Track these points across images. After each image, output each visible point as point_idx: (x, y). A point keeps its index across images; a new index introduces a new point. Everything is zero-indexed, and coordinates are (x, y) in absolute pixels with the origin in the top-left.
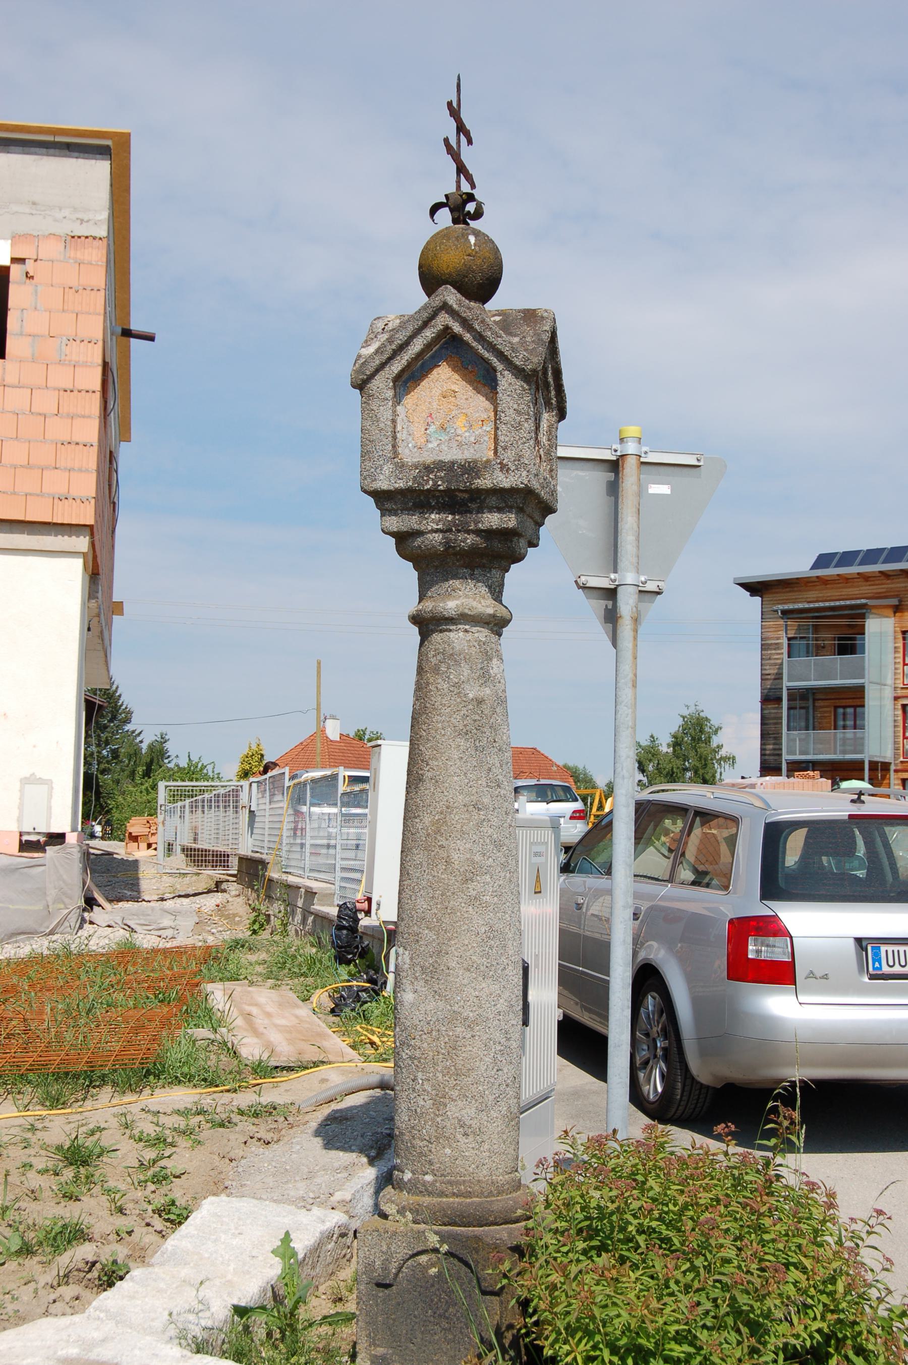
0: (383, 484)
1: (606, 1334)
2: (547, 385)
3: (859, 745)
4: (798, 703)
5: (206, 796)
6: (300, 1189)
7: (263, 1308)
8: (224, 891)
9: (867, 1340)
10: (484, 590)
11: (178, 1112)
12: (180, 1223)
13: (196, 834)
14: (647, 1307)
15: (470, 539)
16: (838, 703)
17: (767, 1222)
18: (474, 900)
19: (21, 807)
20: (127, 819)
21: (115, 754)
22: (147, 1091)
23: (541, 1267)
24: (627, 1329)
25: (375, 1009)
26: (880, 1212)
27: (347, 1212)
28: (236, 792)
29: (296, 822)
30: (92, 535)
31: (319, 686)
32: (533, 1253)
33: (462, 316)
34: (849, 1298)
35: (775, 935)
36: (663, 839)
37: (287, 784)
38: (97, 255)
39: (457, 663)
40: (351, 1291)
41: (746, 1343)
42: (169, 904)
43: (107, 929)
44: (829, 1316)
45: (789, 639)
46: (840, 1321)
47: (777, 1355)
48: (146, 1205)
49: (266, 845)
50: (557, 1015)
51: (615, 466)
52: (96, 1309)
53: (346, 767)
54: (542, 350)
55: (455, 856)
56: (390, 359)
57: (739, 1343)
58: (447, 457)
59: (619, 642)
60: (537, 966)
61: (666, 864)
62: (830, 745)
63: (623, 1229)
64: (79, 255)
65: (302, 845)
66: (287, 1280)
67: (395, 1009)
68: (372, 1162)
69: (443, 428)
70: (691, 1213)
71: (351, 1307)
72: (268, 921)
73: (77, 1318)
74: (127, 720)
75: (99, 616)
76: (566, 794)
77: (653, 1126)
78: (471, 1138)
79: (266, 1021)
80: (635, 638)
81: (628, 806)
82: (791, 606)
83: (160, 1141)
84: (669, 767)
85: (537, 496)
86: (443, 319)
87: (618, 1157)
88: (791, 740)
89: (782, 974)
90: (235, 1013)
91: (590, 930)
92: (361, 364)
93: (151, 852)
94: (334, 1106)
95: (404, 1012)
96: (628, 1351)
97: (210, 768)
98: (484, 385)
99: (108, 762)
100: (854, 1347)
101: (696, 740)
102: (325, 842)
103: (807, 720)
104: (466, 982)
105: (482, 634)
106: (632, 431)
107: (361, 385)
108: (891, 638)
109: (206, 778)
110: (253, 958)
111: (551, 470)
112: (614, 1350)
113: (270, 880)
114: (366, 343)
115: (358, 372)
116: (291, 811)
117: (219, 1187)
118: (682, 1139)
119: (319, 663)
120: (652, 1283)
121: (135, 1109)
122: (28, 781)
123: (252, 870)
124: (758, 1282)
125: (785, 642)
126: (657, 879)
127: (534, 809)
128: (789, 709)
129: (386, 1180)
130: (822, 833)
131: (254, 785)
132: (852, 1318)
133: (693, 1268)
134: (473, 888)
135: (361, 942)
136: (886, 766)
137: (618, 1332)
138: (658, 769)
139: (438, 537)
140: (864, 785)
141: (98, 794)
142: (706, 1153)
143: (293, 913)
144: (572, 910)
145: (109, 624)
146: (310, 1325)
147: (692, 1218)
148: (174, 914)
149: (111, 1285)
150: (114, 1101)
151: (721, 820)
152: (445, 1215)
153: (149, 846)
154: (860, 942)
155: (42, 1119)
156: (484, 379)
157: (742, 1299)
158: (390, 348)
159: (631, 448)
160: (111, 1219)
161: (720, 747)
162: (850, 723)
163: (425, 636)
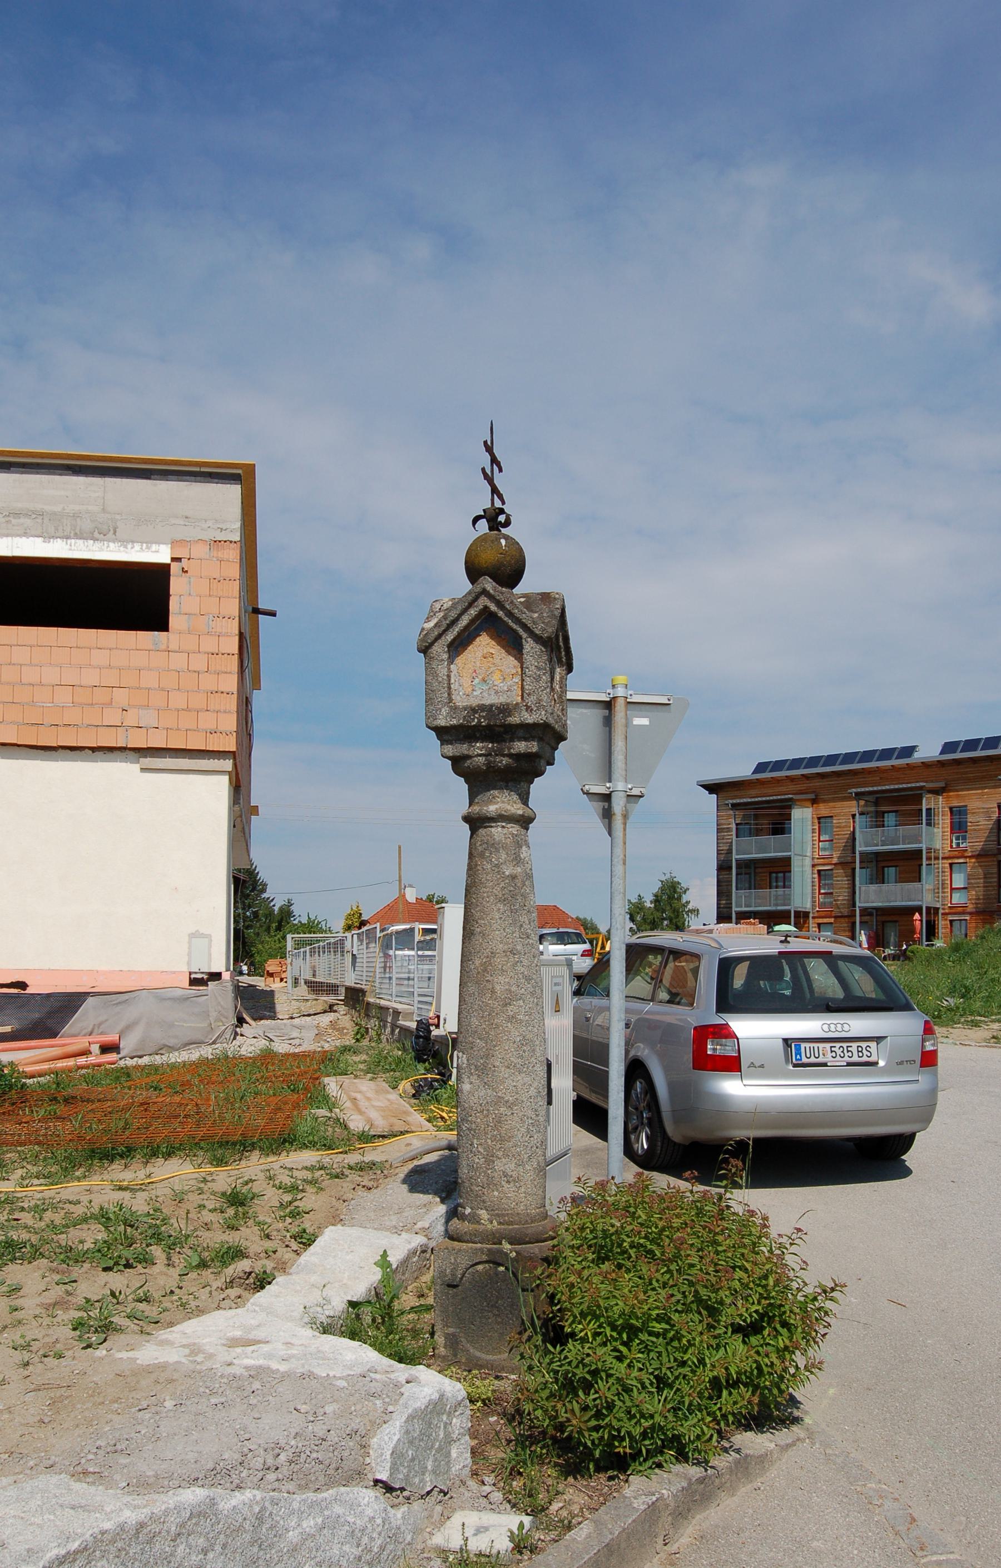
0: (442, 722)
1: (608, 1317)
2: (559, 647)
3: (787, 900)
4: (743, 870)
5: (321, 944)
6: (393, 1220)
7: (369, 1302)
8: (335, 1011)
9: (789, 1317)
10: (515, 797)
11: (306, 1168)
12: (310, 1245)
13: (315, 971)
14: (637, 1298)
15: (505, 761)
16: (772, 869)
17: (720, 1238)
18: (512, 1019)
19: (189, 954)
20: (266, 961)
21: (256, 914)
22: (284, 1153)
23: (563, 1271)
24: (622, 1314)
25: (444, 1093)
26: (799, 1230)
27: (426, 1236)
28: (342, 941)
29: (385, 962)
30: (235, 759)
31: (400, 864)
32: (557, 1263)
33: (498, 599)
34: (777, 1289)
35: (726, 1037)
36: (648, 970)
37: (378, 935)
38: (233, 554)
39: (497, 850)
40: (430, 1289)
41: (705, 1322)
42: (296, 1021)
43: (252, 1040)
44: (763, 1301)
45: (737, 824)
46: (770, 1304)
47: (726, 1328)
48: (285, 1233)
49: (364, 978)
50: (572, 1096)
51: (609, 705)
52: (253, 1304)
53: (421, 922)
54: (555, 622)
55: (498, 987)
56: (445, 631)
57: (700, 1321)
58: (487, 702)
59: (613, 832)
60: (557, 1063)
61: (649, 988)
62: (766, 900)
63: (620, 1246)
64: (220, 555)
65: (390, 978)
66: (385, 1283)
67: (457, 1092)
68: (443, 1201)
69: (484, 680)
70: (667, 1233)
71: (430, 1301)
72: (367, 1032)
73: (239, 1311)
74: (264, 891)
75: (241, 816)
76: (578, 939)
77: (642, 1173)
78: (512, 1184)
79: (367, 1104)
80: (625, 830)
81: (620, 949)
82: (738, 801)
83: (294, 1188)
84: (651, 917)
85: (553, 728)
86: (483, 601)
87: (616, 1195)
88: (738, 897)
89: (732, 1065)
90: (344, 1097)
91: (596, 1036)
92: (424, 635)
93: (283, 984)
94: (416, 1163)
95: (463, 1097)
96: (623, 1328)
97: (323, 923)
98: (514, 649)
99: (251, 921)
100: (780, 1322)
101: (671, 898)
102: (406, 976)
103: (750, 882)
104: (506, 1076)
105: (514, 829)
106: (621, 679)
107: (425, 649)
108: (810, 823)
109: (321, 931)
110: (357, 1059)
111: (563, 710)
112: (614, 1328)
113: (368, 1004)
114: (428, 620)
115: (422, 640)
116: (381, 955)
117: (336, 1219)
118: (662, 1181)
119: (400, 847)
120: (640, 1281)
121: (276, 1166)
122: (193, 936)
123: (355, 997)
124: (713, 1280)
125: (734, 826)
126: (643, 999)
127: (553, 949)
128: (737, 874)
129: (453, 1214)
130: (760, 965)
131: (355, 936)
132: (779, 1302)
133: (669, 1271)
134: (511, 1010)
135: (433, 1046)
136: (806, 915)
137: (616, 1316)
138: (644, 919)
139: (482, 759)
140: (791, 928)
141: (244, 943)
142: (678, 1191)
143: (385, 1026)
144: (581, 1022)
145: (249, 822)
146: (402, 1313)
147: (668, 1237)
148: (300, 1028)
149: (263, 1287)
150: (262, 1161)
151: (688, 957)
152: (495, 1237)
153: (282, 980)
154: (787, 1042)
155: (211, 1174)
156: (513, 645)
157: (703, 1292)
158: (445, 623)
159: (620, 692)
160: (261, 1243)
161: (688, 903)
162: (781, 884)
163: (473, 831)
